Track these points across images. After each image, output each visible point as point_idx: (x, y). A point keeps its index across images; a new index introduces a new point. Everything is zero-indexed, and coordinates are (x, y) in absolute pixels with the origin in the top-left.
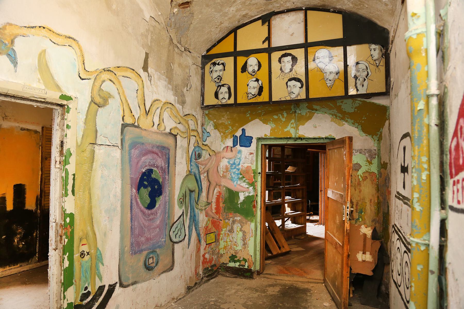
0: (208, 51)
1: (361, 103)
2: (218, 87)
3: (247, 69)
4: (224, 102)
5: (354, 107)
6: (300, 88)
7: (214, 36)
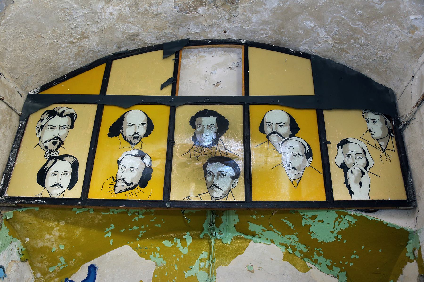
0: (44, 87)
1: (353, 221)
2: (50, 159)
3: (121, 131)
4: (56, 193)
5: (337, 231)
6: (233, 178)
7: (63, 61)
